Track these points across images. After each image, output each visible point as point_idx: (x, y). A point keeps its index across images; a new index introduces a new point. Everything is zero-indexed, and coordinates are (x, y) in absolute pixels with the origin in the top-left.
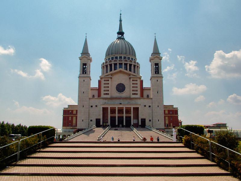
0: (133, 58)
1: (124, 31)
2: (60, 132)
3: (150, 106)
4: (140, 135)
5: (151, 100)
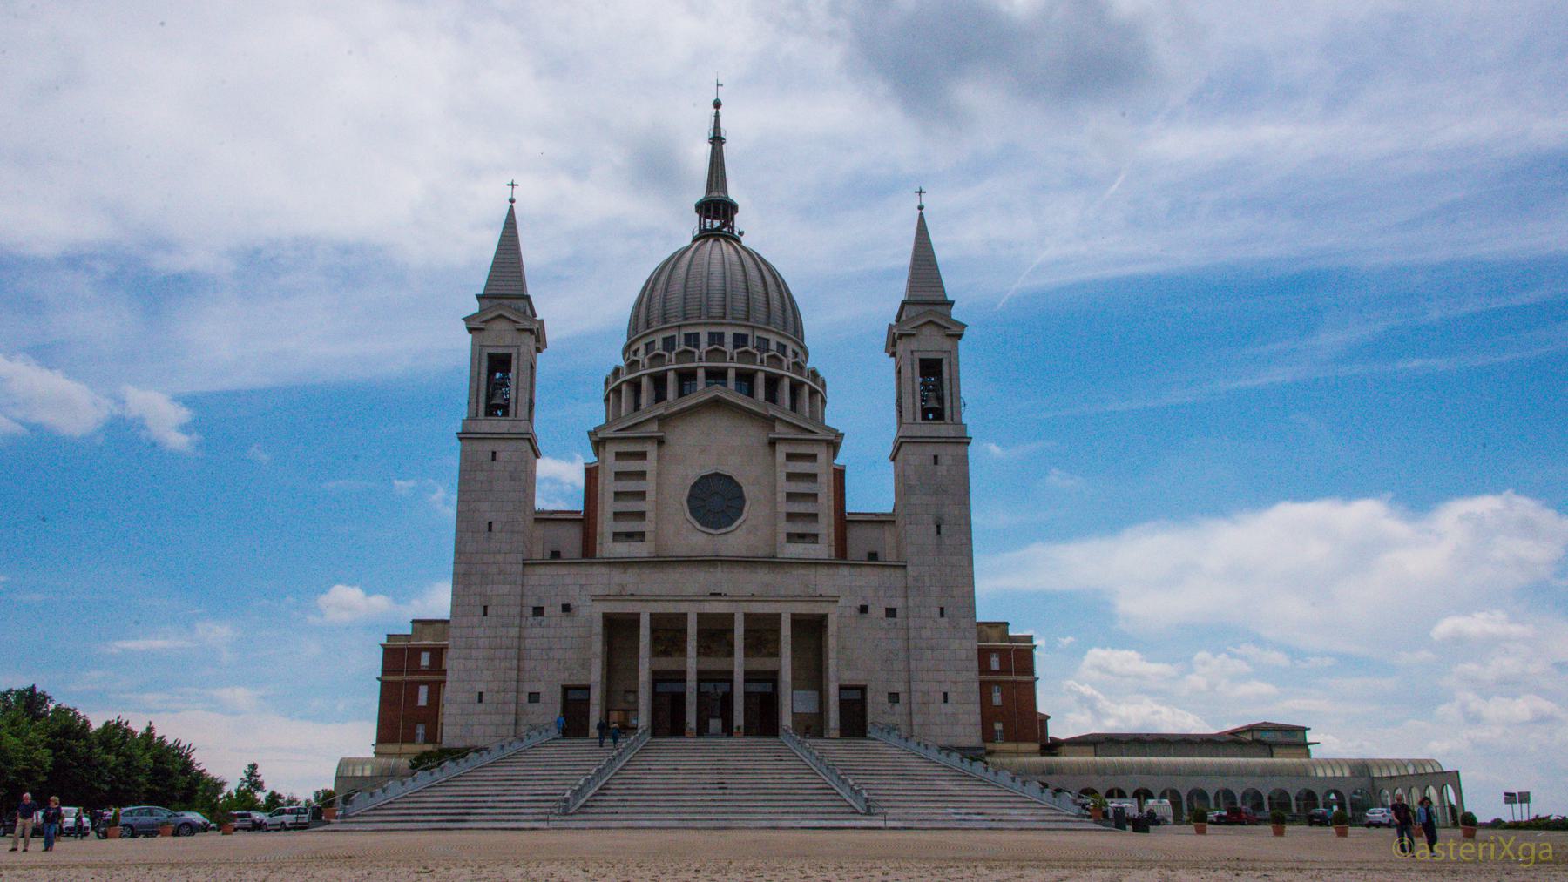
0: (785, 347)
1: (734, 193)
2: (359, 773)
3: (891, 612)
4: (844, 782)
5: (899, 573)
